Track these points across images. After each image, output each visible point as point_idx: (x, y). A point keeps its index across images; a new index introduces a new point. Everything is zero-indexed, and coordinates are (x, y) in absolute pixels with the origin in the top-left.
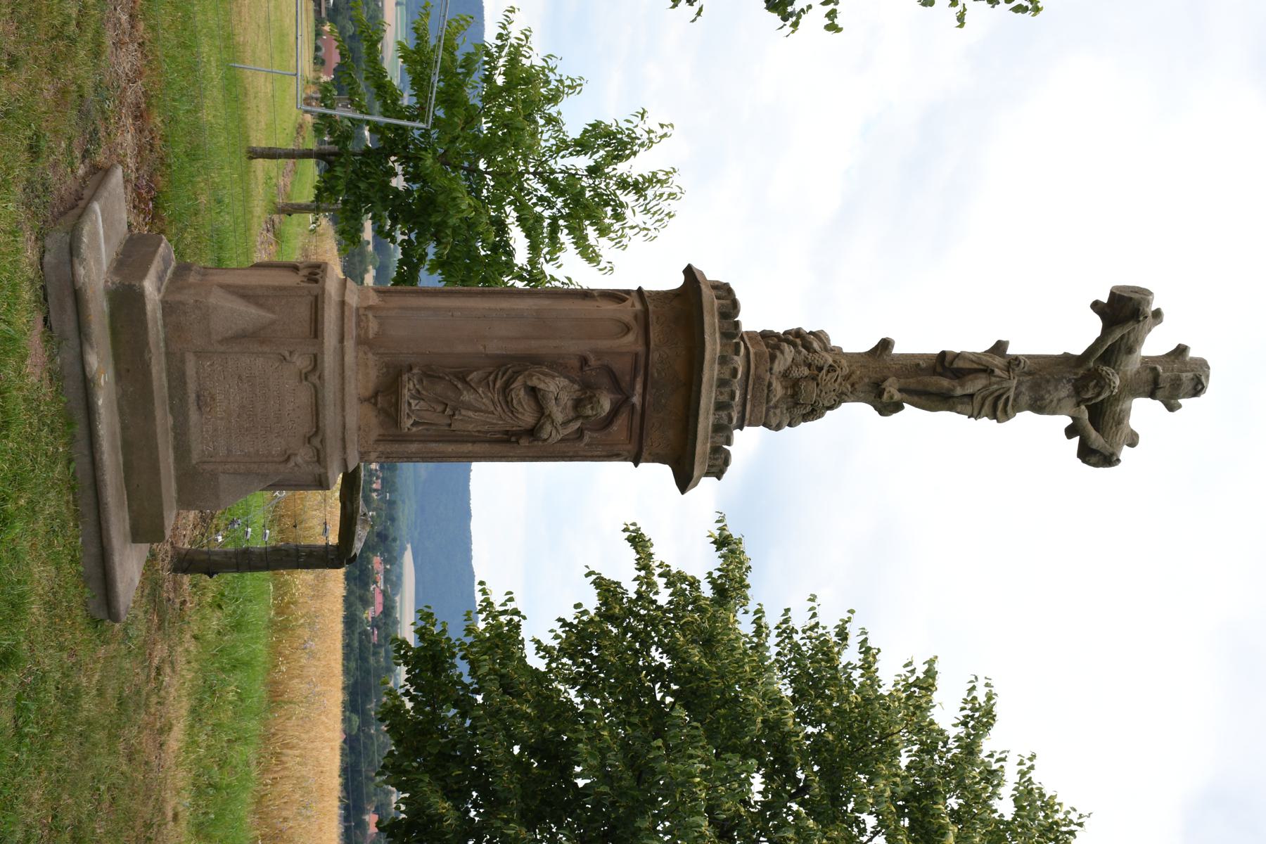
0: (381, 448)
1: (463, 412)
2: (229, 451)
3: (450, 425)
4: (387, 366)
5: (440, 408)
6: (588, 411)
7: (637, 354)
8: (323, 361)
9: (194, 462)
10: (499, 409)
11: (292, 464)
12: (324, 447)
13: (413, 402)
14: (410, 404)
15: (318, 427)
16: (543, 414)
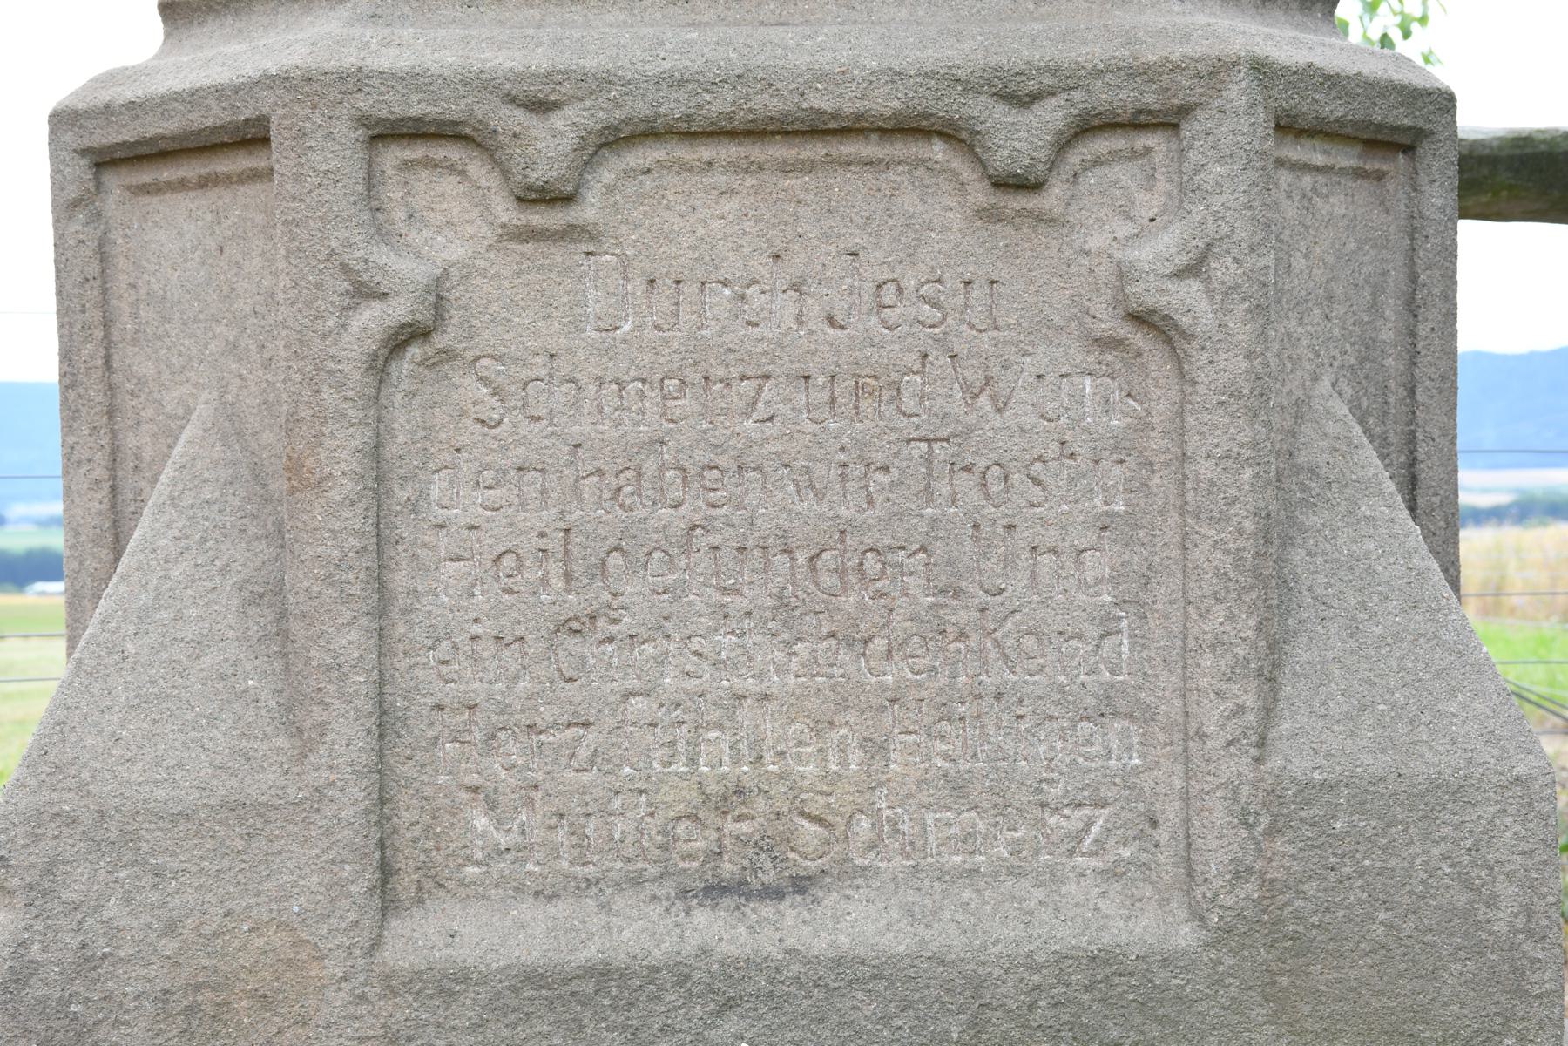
2: (1106, 709)
8: (414, 80)
9: (1185, 936)
11: (1189, 301)
12: (1062, 80)
15: (910, 127)
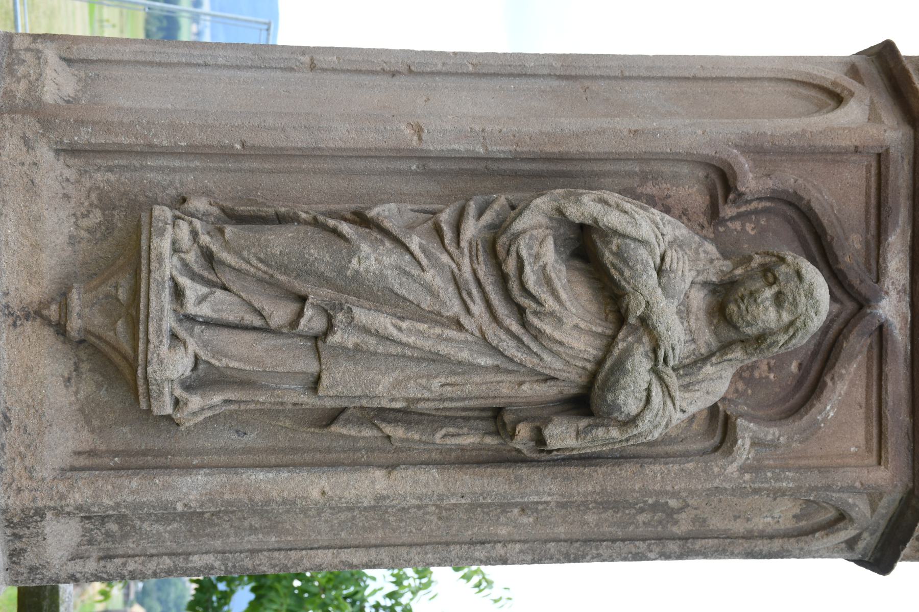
0: (81, 494)
1: (362, 316)
3: (315, 384)
4: (105, 203)
5: (280, 313)
6: (767, 315)
7: (882, 158)
10: (478, 308)
13: (192, 290)
14: (178, 293)
16: (621, 320)
